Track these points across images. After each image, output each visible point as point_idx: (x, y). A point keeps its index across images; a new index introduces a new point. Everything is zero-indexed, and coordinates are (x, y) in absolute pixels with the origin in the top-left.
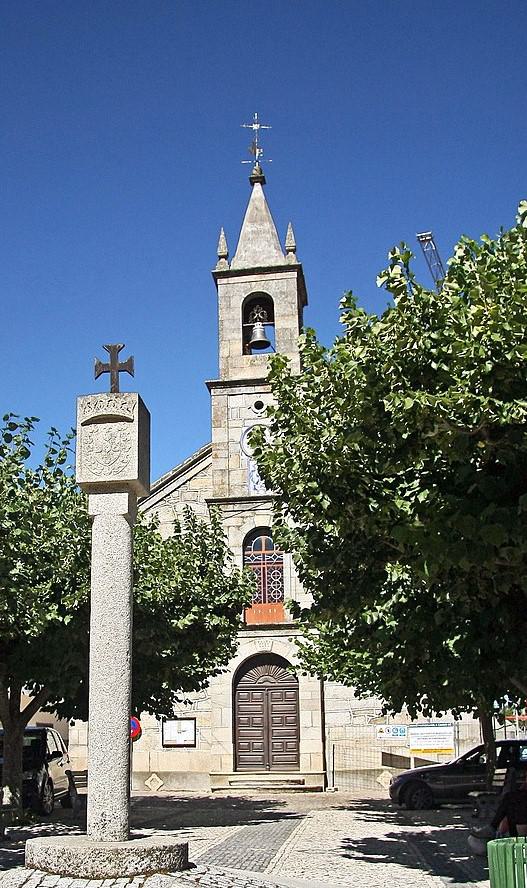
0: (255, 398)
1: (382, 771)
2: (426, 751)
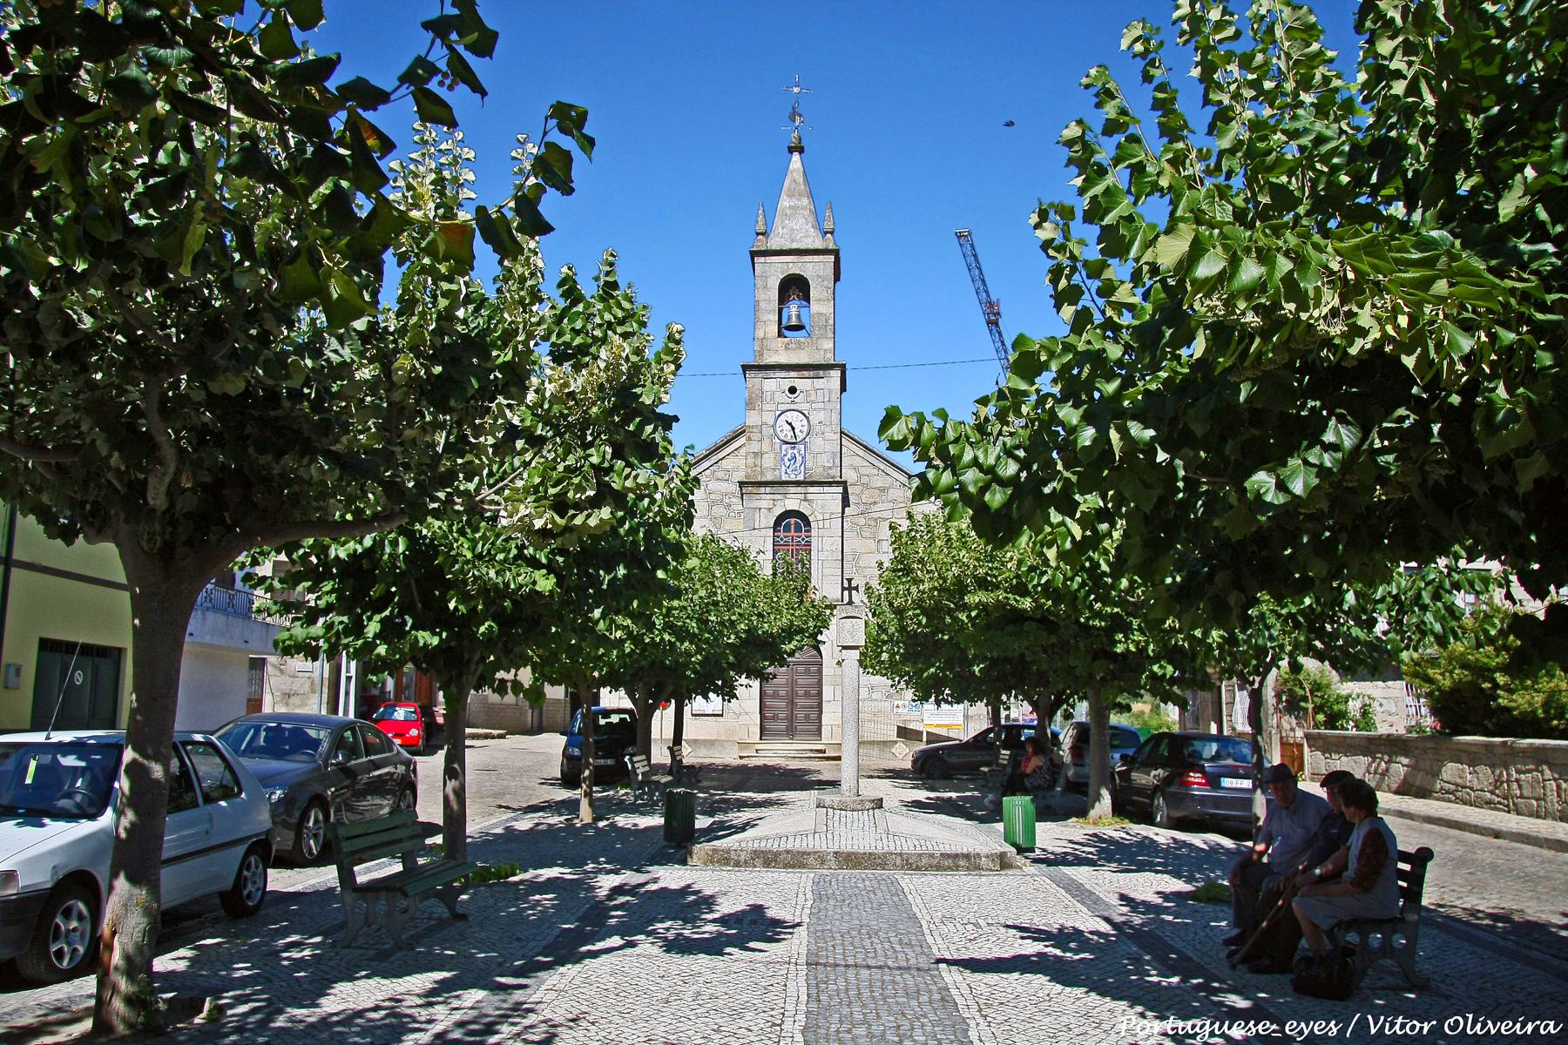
0: (787, 384)
1: (896, 742)
2: (937, 726)
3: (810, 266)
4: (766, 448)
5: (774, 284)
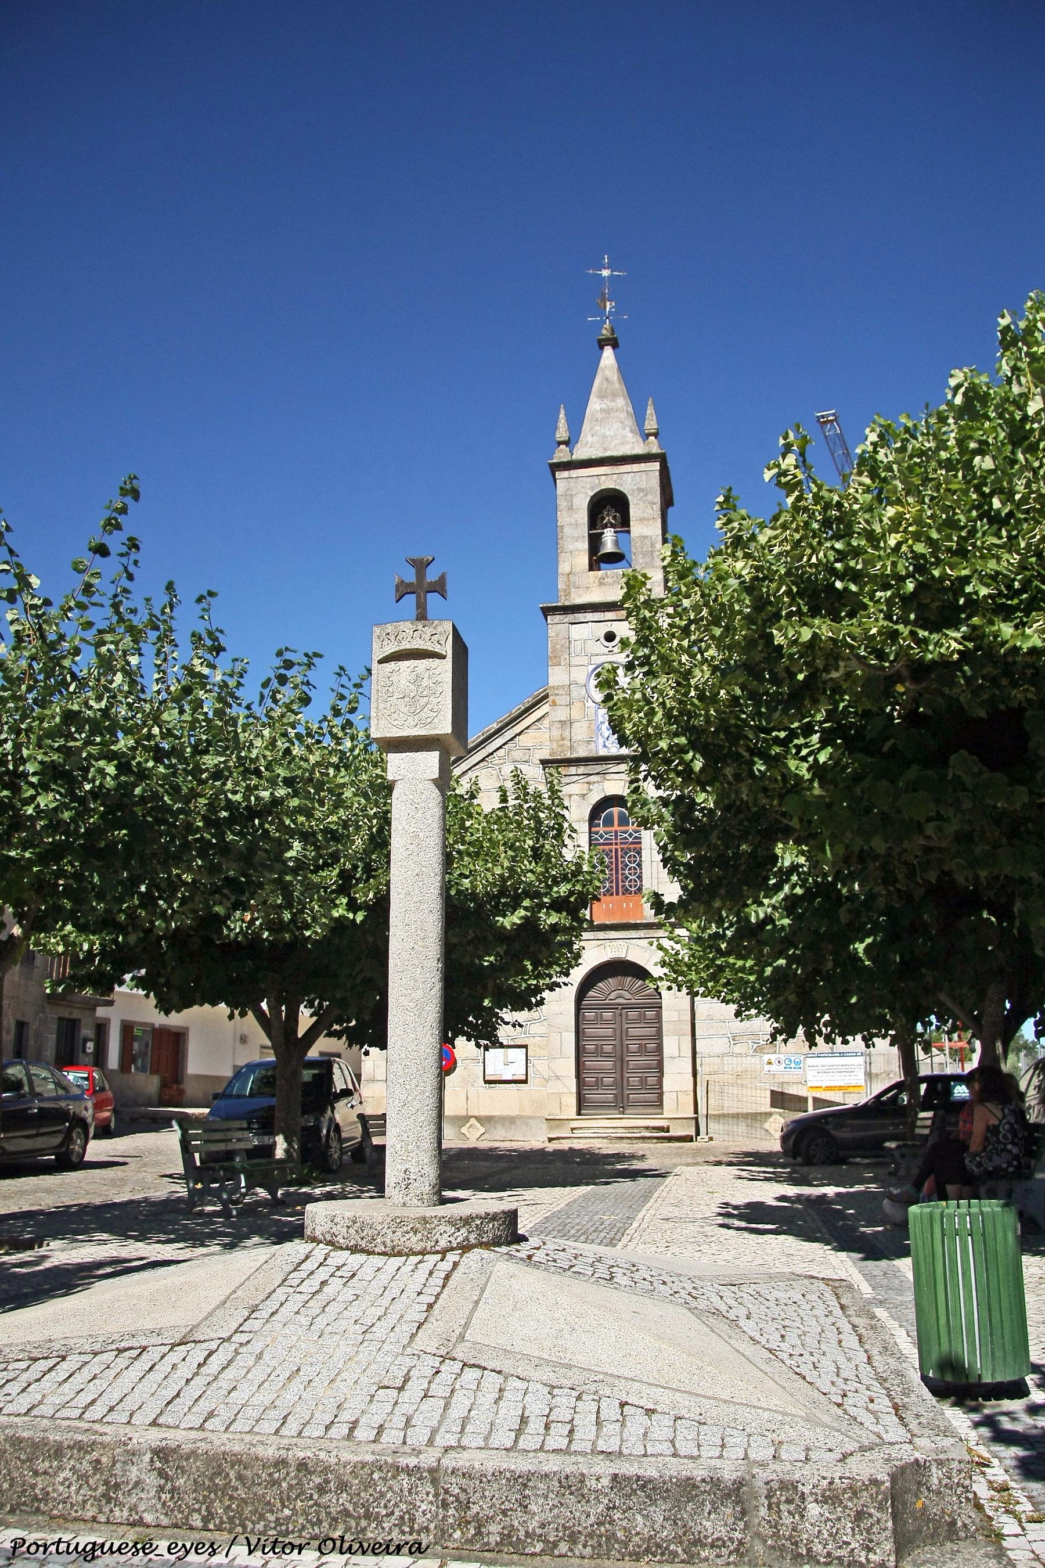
0: (605, 628)
1: (770, 1114)
2: (828, 1088)
3: (628, 478)
4: (575, 714)
5: (582, 503)
